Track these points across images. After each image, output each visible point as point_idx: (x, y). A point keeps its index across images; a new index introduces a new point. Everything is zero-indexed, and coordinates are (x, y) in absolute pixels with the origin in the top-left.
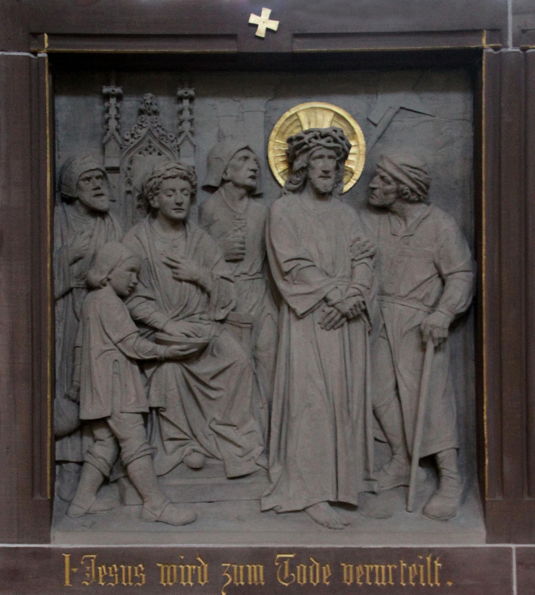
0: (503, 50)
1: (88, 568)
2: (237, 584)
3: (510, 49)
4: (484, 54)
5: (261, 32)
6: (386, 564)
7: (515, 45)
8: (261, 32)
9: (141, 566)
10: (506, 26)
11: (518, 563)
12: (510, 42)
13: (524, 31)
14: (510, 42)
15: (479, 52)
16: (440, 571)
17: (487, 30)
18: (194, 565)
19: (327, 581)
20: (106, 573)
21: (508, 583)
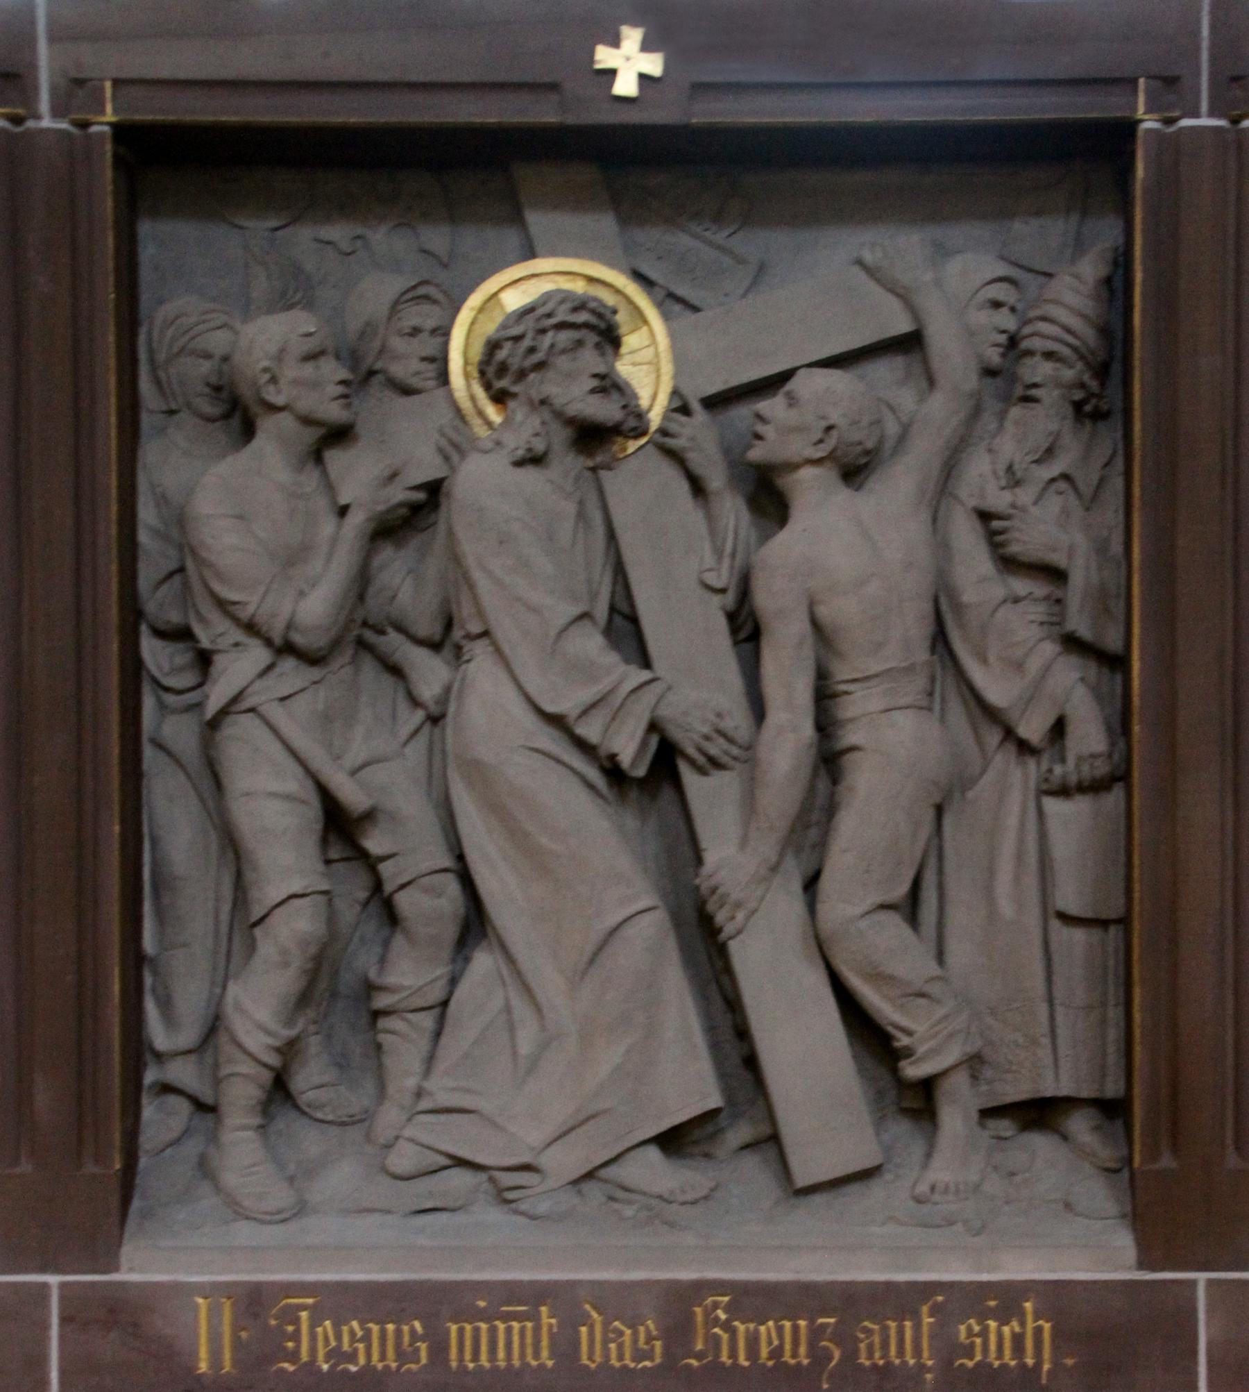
0: (30, 124)
1: (290, 1328)
2: (380, 1366)
3: (47, 123)
4: (1140, 134)
5: (626, 86)
6: (382, 1323)
7: (57, 113)
8: (626, 86)
9: (972, 1321)
10: (33, 66)
11: (65, 1320)
12: (44, 105)
13: (79, 82)
14: (44, 105)
15: (1126, 129)
16: (552, 1336)
17: (1148, 77)
18: (752, 1321)
19: (770, 1358)
20: (333, 1343)
21: (38, 1363)
